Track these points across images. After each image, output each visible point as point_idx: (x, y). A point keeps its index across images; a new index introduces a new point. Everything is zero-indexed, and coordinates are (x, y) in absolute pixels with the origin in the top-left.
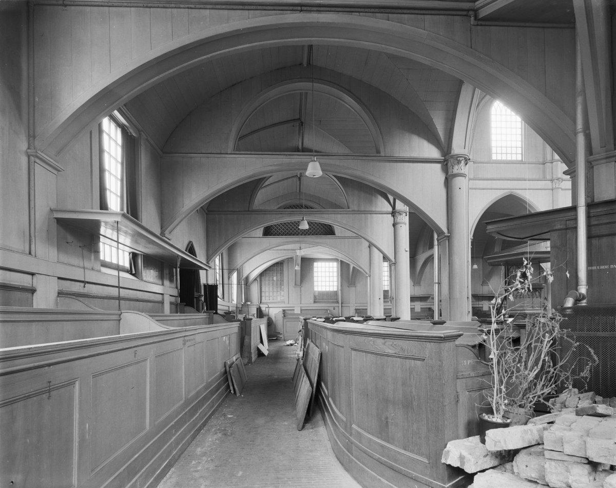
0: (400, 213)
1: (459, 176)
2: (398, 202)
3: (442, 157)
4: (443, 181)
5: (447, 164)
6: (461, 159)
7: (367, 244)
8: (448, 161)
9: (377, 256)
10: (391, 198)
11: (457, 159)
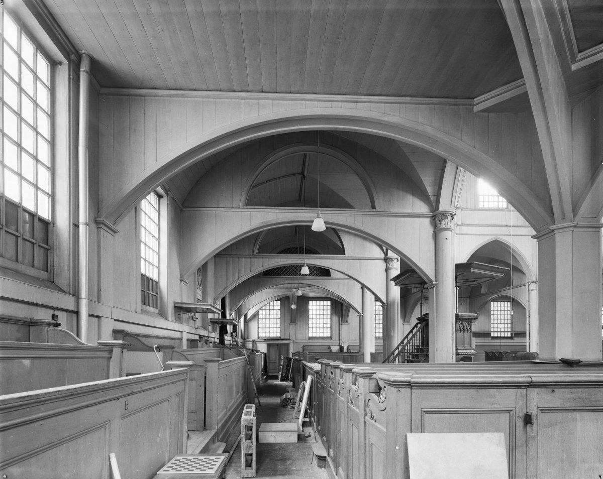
0: (391, 259)
1: (446, 230)
2: (389, 251)
3: (431, 212)
4: (432, 234)
5: (435, 219)
6: (447, 215)
7: (360, 286)
8: (437, 218)
9: (369, 297)
10: (384, 248)
11: (444, 215)
